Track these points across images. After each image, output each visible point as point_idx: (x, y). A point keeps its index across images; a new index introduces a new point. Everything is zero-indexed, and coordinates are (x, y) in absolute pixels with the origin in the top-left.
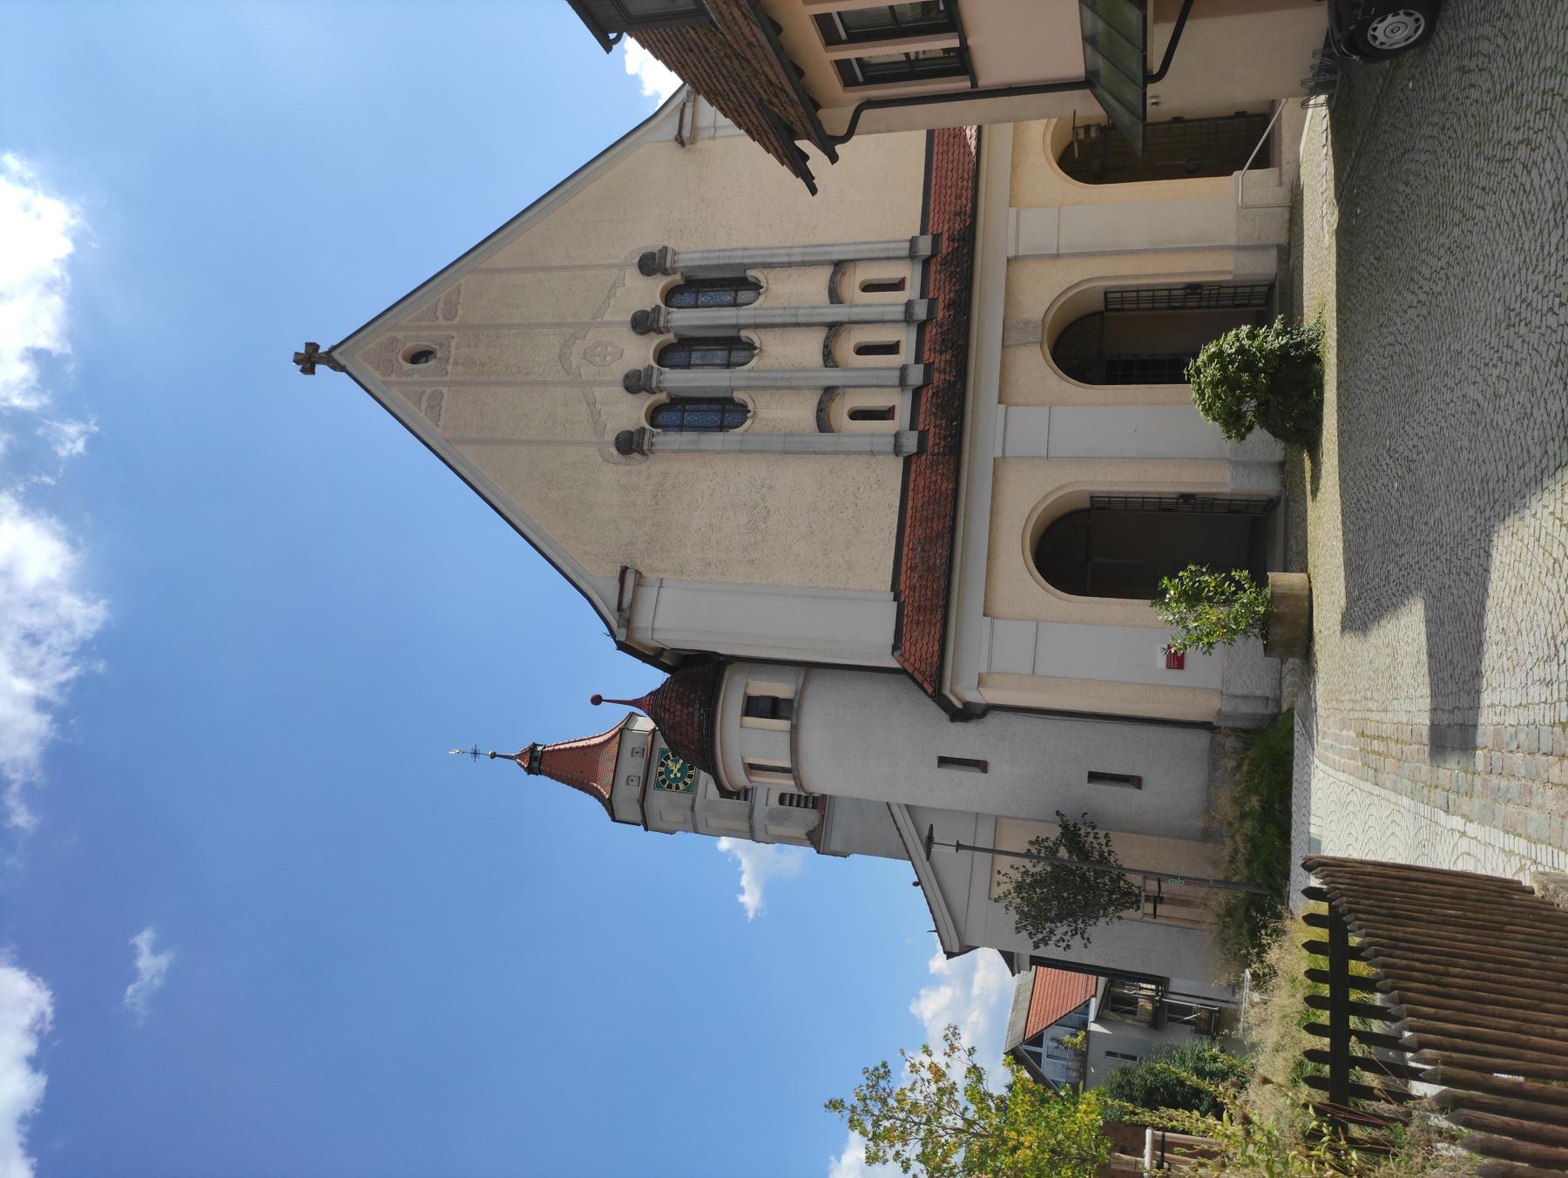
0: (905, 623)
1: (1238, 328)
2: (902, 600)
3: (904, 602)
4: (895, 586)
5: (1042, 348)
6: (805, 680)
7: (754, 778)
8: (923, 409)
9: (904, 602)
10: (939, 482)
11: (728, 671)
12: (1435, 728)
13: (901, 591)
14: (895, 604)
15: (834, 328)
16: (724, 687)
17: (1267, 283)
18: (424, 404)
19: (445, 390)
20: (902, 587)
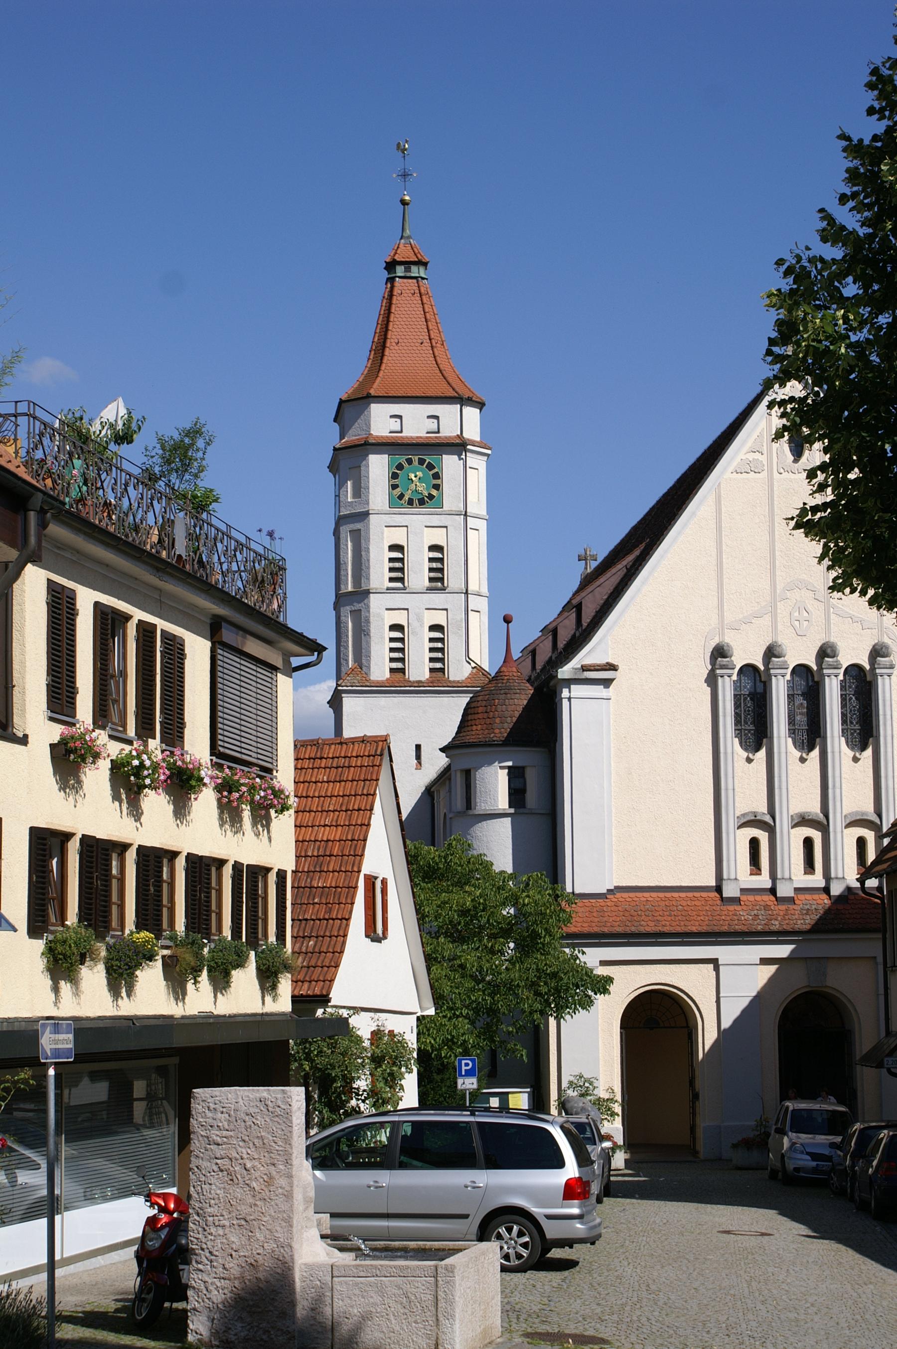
0: (591, 901)
1: (773, 387)
2: (608, 896)
3: (607, 898)
4: (619, 889)
5: (806, 987)
6: (543, 814)
7: (459, 774)
8: (758, 898)
9: (607, 898)
10: (699, 918)
11: (543, 750)
12: (876, 1067)
13: (615, 894)
14: (605, 891)
15: (823, 827)
16: (534, 749)
17: (420, 257)
18: (751, 456)
19: (764, 474)
20: (618, 895)
